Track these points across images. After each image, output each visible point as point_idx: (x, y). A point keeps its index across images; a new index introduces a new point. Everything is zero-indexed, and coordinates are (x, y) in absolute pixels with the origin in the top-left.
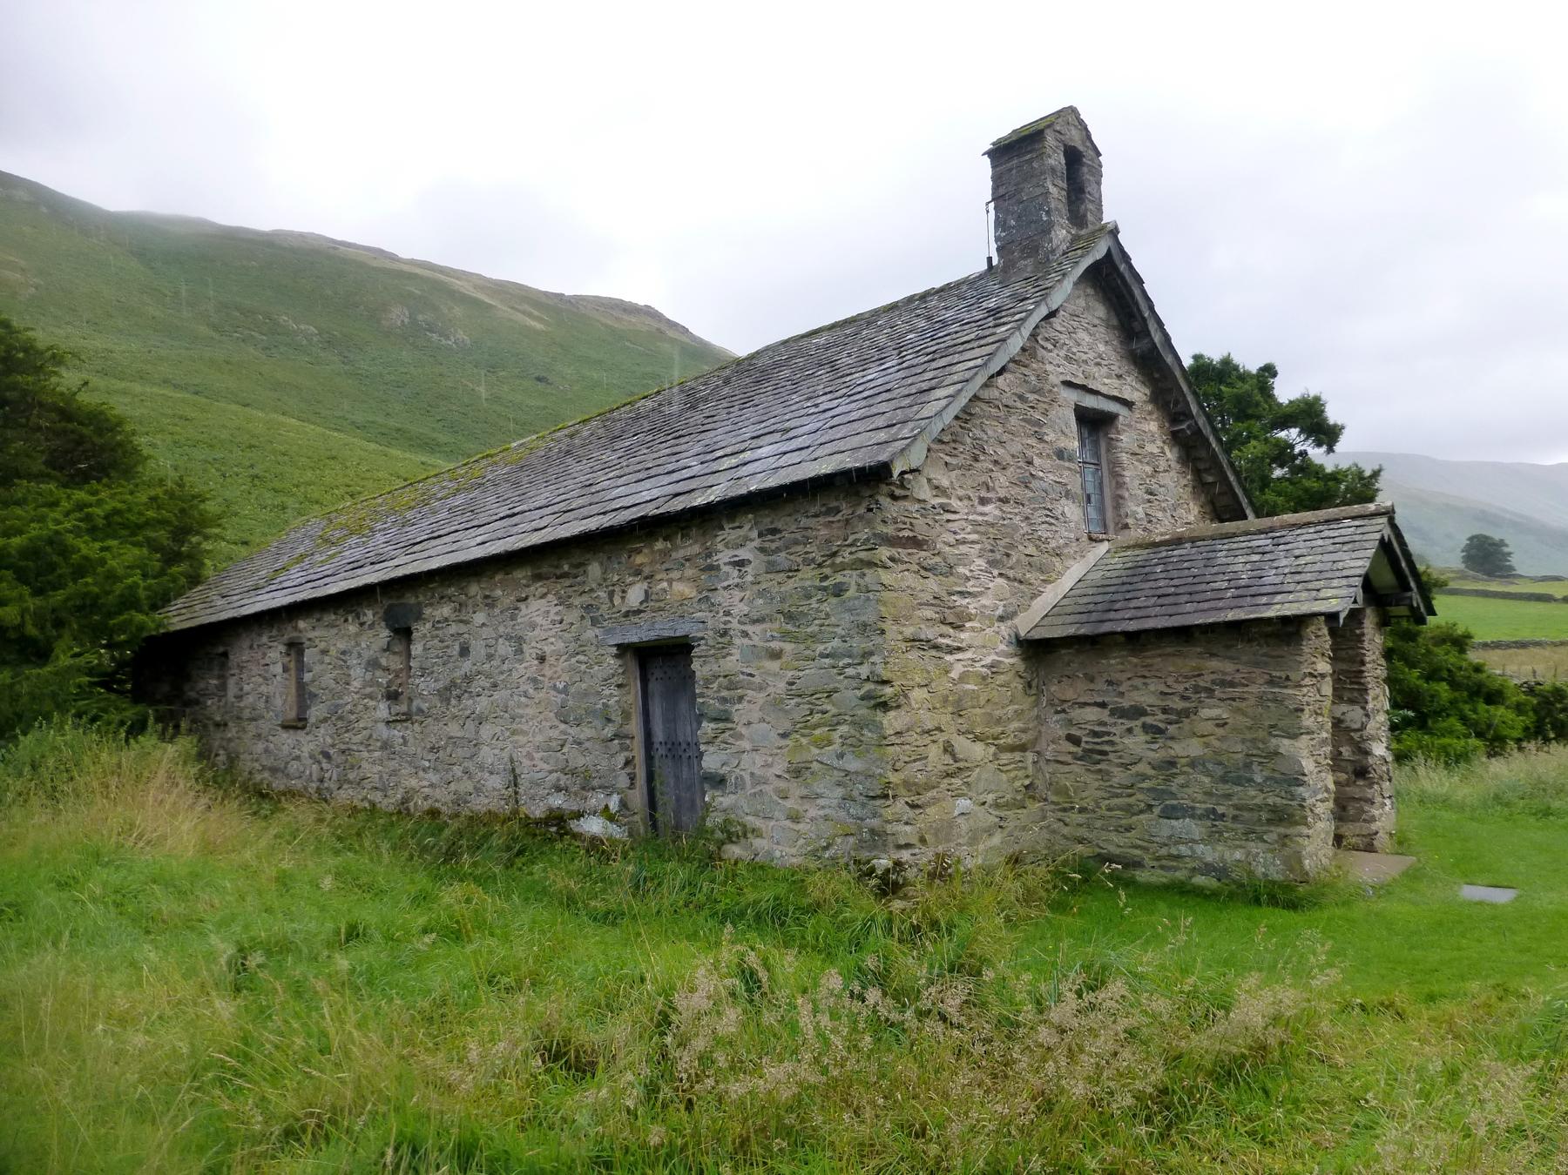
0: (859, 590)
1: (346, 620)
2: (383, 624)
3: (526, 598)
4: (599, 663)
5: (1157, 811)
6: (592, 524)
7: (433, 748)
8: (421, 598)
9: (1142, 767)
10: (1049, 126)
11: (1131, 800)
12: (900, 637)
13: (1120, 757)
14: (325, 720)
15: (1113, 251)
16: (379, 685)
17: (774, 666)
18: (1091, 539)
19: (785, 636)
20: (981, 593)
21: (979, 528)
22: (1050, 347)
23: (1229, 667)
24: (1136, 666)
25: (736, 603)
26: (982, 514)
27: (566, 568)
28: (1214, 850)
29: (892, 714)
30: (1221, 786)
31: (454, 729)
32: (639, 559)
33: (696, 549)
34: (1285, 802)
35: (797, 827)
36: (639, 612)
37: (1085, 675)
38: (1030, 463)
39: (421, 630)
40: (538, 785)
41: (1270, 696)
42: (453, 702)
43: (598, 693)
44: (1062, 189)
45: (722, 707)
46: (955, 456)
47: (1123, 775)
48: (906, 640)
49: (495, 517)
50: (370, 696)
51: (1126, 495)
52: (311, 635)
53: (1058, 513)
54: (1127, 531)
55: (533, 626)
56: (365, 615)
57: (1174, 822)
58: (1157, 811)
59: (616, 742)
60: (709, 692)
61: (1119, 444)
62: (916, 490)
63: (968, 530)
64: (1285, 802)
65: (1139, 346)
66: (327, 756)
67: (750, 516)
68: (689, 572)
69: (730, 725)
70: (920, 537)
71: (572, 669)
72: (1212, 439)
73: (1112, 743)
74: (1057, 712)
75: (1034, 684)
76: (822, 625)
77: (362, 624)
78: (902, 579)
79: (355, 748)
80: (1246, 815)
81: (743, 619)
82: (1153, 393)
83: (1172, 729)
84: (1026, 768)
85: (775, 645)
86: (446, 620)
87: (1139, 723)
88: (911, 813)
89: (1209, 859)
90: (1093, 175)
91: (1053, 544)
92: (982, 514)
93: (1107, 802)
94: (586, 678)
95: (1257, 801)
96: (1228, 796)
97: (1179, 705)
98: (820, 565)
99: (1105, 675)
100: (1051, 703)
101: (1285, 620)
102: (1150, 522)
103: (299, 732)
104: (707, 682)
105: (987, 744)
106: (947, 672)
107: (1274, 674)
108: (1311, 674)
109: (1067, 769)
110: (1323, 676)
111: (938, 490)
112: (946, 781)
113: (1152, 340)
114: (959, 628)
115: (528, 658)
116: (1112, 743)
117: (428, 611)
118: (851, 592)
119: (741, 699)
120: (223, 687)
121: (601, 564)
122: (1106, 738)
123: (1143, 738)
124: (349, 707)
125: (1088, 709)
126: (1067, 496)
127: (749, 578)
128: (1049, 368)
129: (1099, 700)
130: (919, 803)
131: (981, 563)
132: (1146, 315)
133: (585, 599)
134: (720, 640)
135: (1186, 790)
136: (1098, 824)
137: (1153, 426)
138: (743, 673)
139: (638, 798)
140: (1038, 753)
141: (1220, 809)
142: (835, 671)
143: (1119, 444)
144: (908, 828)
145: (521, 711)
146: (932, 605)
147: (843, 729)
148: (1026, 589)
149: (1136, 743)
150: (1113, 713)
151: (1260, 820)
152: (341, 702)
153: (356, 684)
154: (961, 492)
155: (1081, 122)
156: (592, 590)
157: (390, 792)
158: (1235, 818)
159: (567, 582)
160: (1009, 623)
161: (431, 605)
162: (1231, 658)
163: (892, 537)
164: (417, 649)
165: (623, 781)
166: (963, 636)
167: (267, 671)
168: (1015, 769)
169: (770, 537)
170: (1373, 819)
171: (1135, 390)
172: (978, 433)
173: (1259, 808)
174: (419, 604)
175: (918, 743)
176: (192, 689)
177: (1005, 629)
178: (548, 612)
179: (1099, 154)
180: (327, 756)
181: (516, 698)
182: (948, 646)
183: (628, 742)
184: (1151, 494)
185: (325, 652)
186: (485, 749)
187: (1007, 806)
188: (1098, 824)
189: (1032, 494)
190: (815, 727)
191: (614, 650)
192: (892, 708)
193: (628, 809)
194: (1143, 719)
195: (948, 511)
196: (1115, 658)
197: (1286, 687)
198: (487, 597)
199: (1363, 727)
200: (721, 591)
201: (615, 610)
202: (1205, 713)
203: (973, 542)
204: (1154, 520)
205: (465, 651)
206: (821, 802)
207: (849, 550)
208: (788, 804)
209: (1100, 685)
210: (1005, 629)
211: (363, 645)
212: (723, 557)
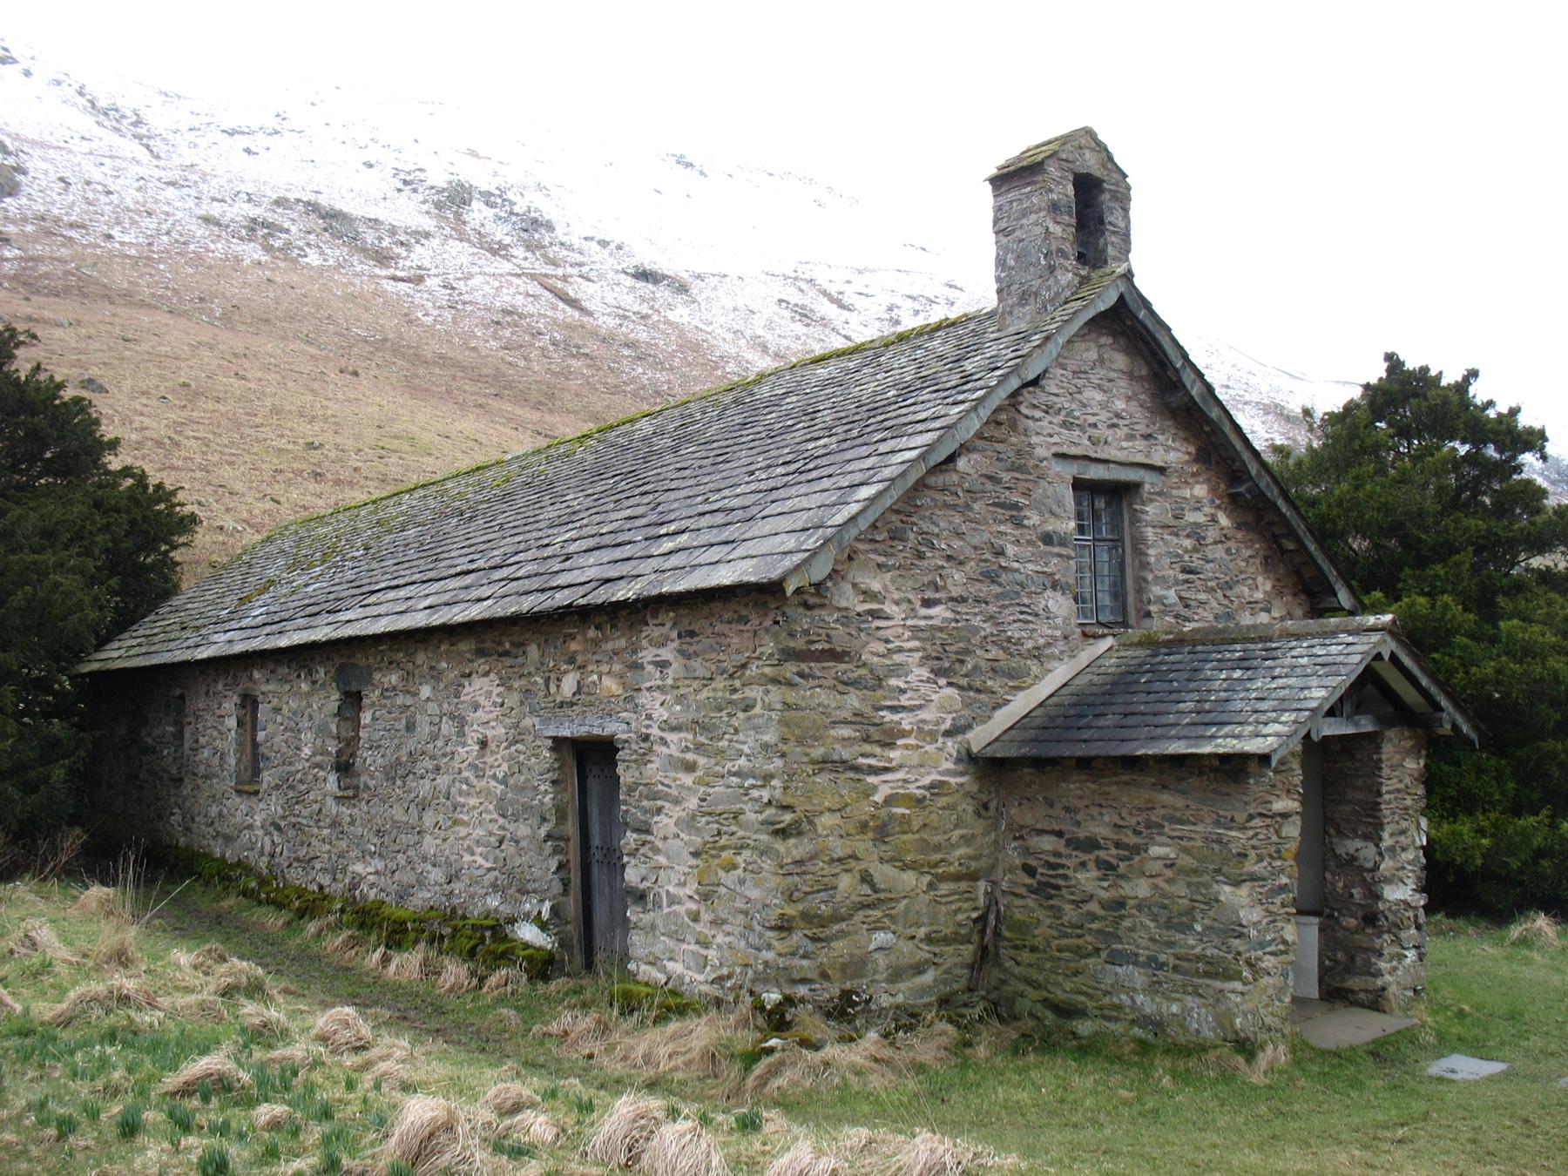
0: (763, 707)
1: (299, 676)
2: (334, 685)
3: (470, 675)
4: (536, 756)
5: (1104, 954)
6: (526, 604)
7: (379, 831)
8: (371, 660)
9: (1093, 907)
10: (1053, 155)
11: (1080, 942)
12: (806, 759)
13: (1072, 893)
14: (277, 787)
15: (1127, 297)
16: (329, 753)
17: (688, 779)
18: (1085, 635)
19: (699, 748)
20: (920, 707)
21: (920, 634)
22: (1038, 414)
23: (1179, 802)
24: (1094, 792)
25: (657, 707)
26: (925, 618)
27: (507, 645)
28: (1153, 1000)
29: (792, 841)
30: (1165, 932)
31: (398, 813)
32: (574, 646)
33: (622, 643)
34: (1221, 954)
35: (704, 952)
36: (572, 704)
37: (1045, 798)
38: (1000, 553)
39: (372, 696)
40: (477, 882)
41: (1214, 837)
42: (399, 782)
43: (536, 788)
44: (1069, 225)
45: (643, 818)
46: (892, 555)
47: (1073, 913)
48: (812, 762)
49: (453, 571)
50: (318, 766)
51: (1150, 577)
52: (265, 688)
53: (1039, 608)
54: (1147, 622)
55: (476, 707)
56: (317, 672)
57: (1118, 969)
58: (1104, 954)
59: (549, 843)
60: (631, 800)
61: (1145, 517)
62: (837, 597)
63: (906, 636)
64: (1221, 954)
65: (1175, 399)
66: (278, 828)
67: (672, 614)
68: (617, 668)
69: (649, 838)
70: (839, 649)
71: (511, 758)
72: (1280, 502)
73: (1065, 877)
74: (1015, 838)
75: (993, 805)
76: (731, 741)
77: (314, 683)
78: (812, 696)
79: (305, 822)
80: (1185, 964)
81: (663, 725)
82: (1199, 450)
83: (1122, 866)
84: (974, 900)
85: (690, 756)
86: (394, 688)
87: (1092, 857)
88: (811, 947)
89: (1148, 1010)
90: (1117, 199)
91: (1029, 645)
92: (925, 618)
93: (1057, 942)
94: (525, 771)
95: (1197, 951)
96: (1170, 944)
97: (1132, 840)
98: (731, 676)
99: (1064, 800)
100: (1010, 827)
101: (1225, 758)
102: (1187, 606)
103: (253, 798)
104: (631, 789)
105: (922, 873)
106: (869, 796)
107: (1221, 813)
108: (1261, 815)
109: (1019, 902)
110: (1285, 815)
111: (868, 595)
112: (861, 913)
113: (1187, 393)
114: (890, 745)
115: (470, 742)
116: (1065, 877)
117: (377, 676)
118: (757, 710)
119: (659, 810)
120: (179, 735)
121: (539, 646)
122: (1061, 871)
123: (1095, 873)
124: (299, 776)
125: (1046, 838)
126: (1054, 587)
127: (670, 681)
128: (1034, 440)
129: (1057, 828)
130: (822, 936)
131: (925, 673)
132: (1178, 365)
133: (523, 682)
134: (643, 745)
135: (1133, 934)
136: (1048, 965)
137: (1200, 490)
138: (663, 784)
139: (572, 906)
140: (993, 882)
141: (1162, 958)
142: (741, 791)
143: (1145, 517)
144: (805, 963)
145: (462, 800)
146: (851, 723)
147: (746, 853)
148: (978, 697)
149: (1087, 879)
150: (1069, 843)
151: (1197, 972)
152: (292, 769)
153: (307, 751)
154: (896, 596)
155: (1099, 144)
156: (530, 674)
157: (339, 876)
158: (1176, 968)
159: (508, 661)
160: (960, 738)
161: (380, 669)
162: (1183, 792)
163: (803, 651)
164: (366, 717)
165: (557, 887)
166: (892, 754)
167: (222, 724)
168: (959, 900)
169: (688, 639)
170: (1379, 974)
171: (1172, 451)
172: (925, 526)
173: (1198, 958)
174: (369, 666)
175: (824, 873)
176: (149, 734)
177: (951, 745)
178: (491, 692)
179: (1125, 176)
180: (278, 828)
181: (457, 784)
182: (870, 766)
183: (562, 844)
184: (1191, 572)
185: (278, 710)
186: (428, 839)
187: (946, 940)
188: (1048, 965)
189: (1000, 590)
190: (723, 848)
191: (549, 743)
192: (791, 835)
193: (559, 917)
194: (1097, 852)
195: (878, 618)
196: (1074, 782)
197: (1231, 829)
198: (432, 668)
199: (1376, 867)
200: (645, 692)
201: (550, 699)
202: (1155, 851)
203: (910, 650)
204: (1193, 603)
205: (411, 727)
206: (726, 928)
207: (757, 663)
208: (699, 927)
209: (1058, 811)
210: (951, 745)
211: (315, 706)
212: (647, 655)
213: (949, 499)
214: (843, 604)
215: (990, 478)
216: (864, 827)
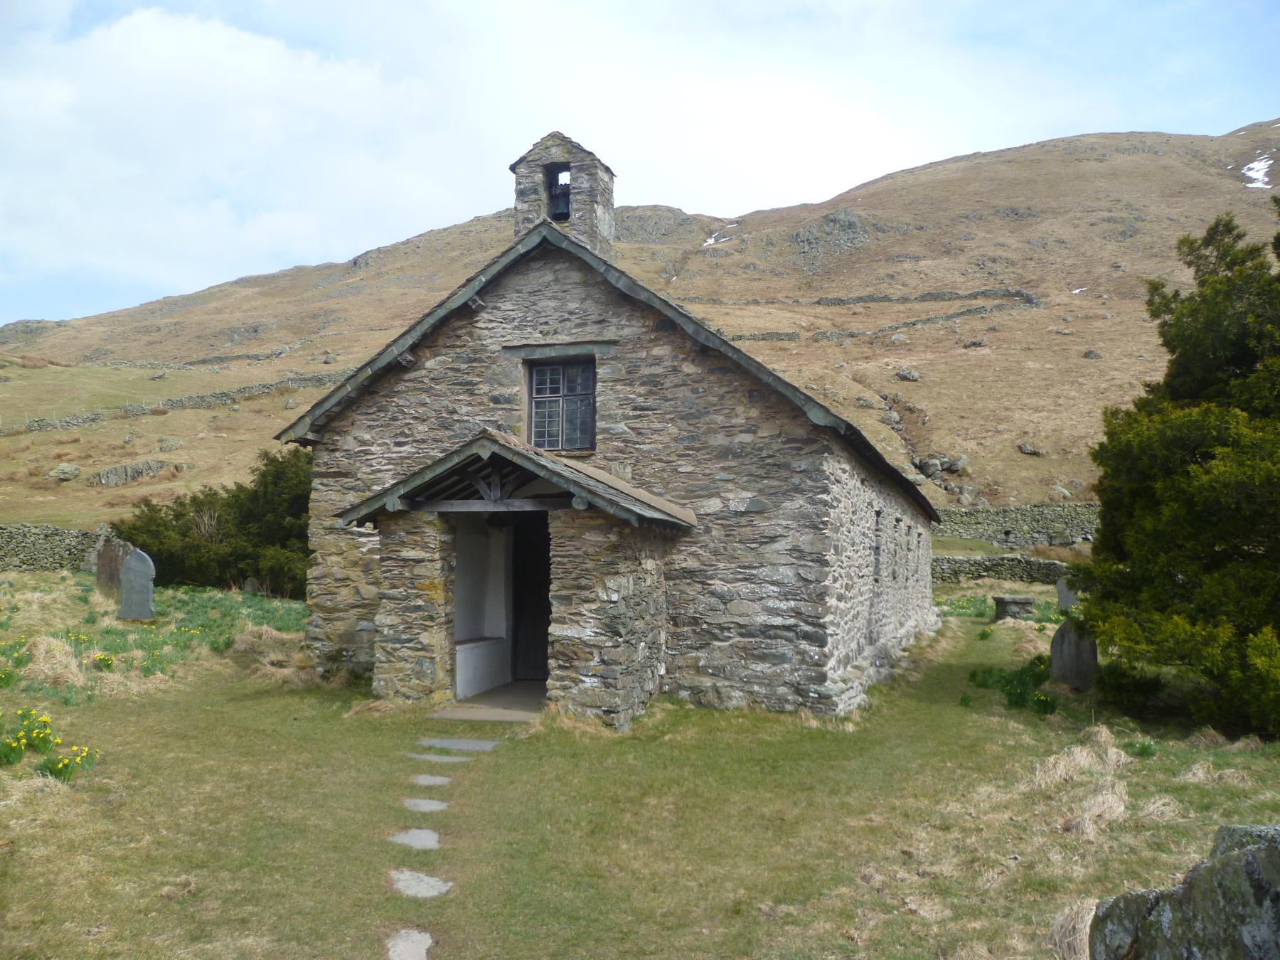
48: (324, 528)
111: (363, 443)
144: (317, 630)
213: (419, 386)
214: (346, 448)
215: (452, 369)
216: (355, 564)
